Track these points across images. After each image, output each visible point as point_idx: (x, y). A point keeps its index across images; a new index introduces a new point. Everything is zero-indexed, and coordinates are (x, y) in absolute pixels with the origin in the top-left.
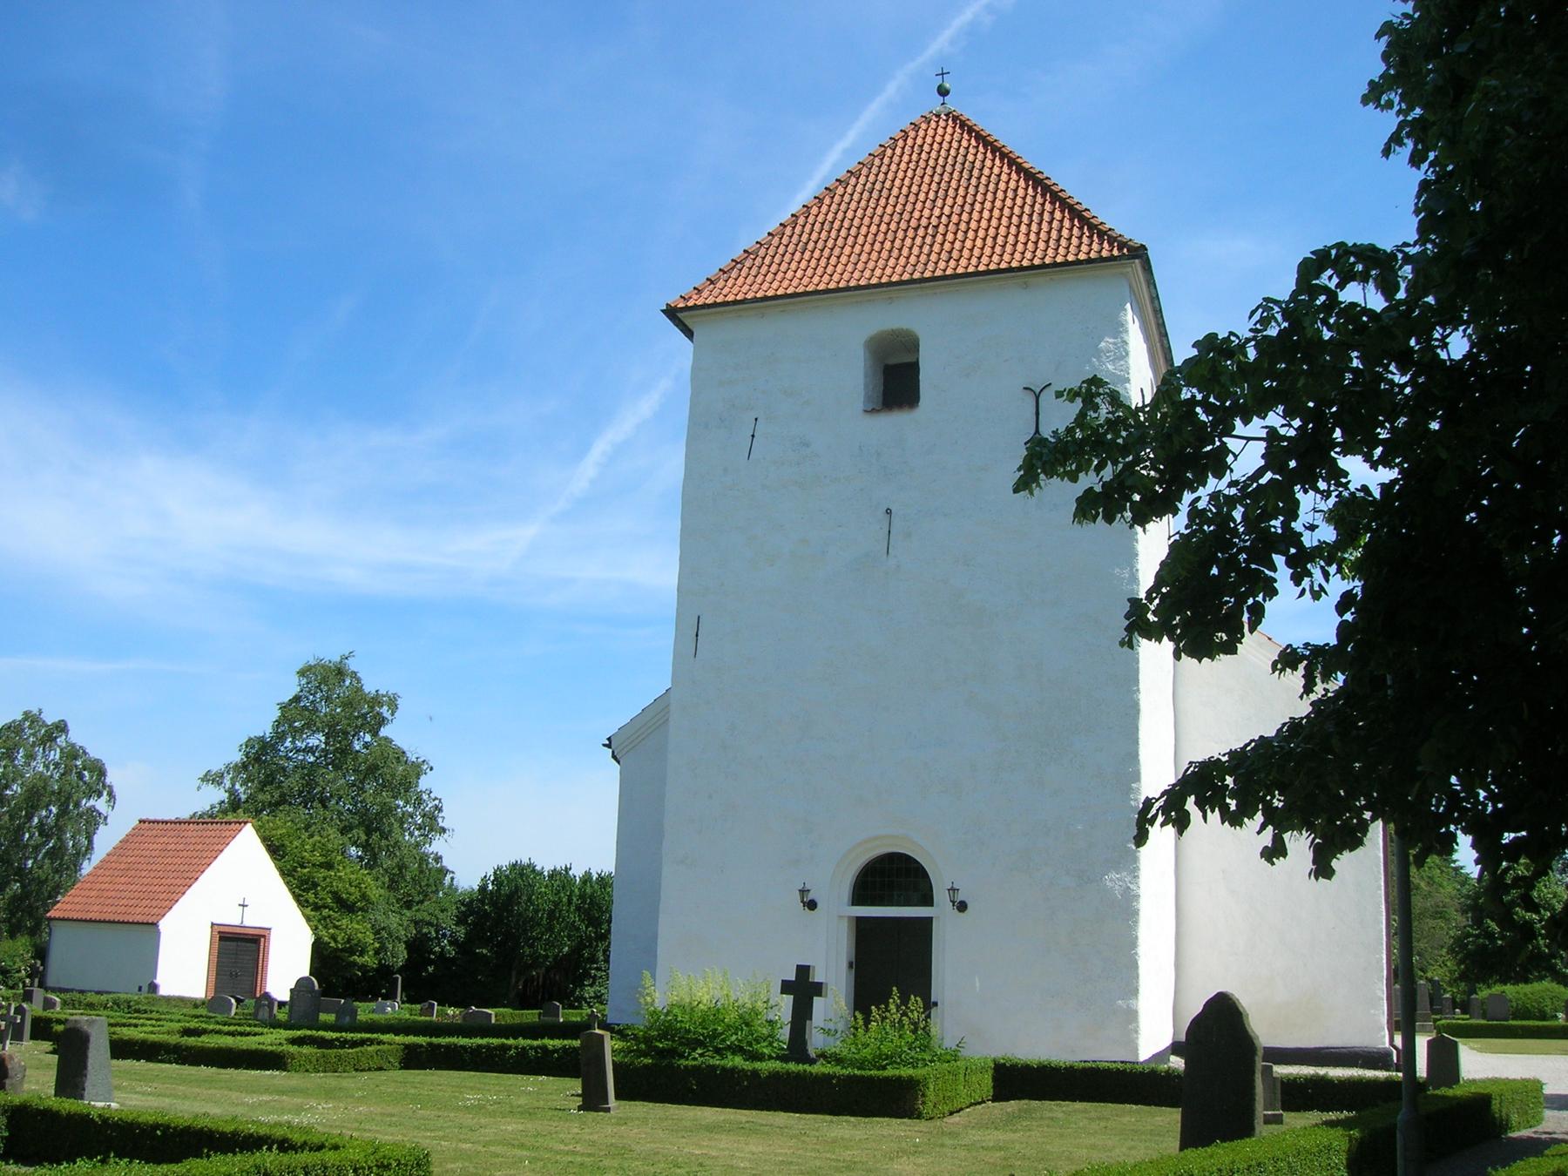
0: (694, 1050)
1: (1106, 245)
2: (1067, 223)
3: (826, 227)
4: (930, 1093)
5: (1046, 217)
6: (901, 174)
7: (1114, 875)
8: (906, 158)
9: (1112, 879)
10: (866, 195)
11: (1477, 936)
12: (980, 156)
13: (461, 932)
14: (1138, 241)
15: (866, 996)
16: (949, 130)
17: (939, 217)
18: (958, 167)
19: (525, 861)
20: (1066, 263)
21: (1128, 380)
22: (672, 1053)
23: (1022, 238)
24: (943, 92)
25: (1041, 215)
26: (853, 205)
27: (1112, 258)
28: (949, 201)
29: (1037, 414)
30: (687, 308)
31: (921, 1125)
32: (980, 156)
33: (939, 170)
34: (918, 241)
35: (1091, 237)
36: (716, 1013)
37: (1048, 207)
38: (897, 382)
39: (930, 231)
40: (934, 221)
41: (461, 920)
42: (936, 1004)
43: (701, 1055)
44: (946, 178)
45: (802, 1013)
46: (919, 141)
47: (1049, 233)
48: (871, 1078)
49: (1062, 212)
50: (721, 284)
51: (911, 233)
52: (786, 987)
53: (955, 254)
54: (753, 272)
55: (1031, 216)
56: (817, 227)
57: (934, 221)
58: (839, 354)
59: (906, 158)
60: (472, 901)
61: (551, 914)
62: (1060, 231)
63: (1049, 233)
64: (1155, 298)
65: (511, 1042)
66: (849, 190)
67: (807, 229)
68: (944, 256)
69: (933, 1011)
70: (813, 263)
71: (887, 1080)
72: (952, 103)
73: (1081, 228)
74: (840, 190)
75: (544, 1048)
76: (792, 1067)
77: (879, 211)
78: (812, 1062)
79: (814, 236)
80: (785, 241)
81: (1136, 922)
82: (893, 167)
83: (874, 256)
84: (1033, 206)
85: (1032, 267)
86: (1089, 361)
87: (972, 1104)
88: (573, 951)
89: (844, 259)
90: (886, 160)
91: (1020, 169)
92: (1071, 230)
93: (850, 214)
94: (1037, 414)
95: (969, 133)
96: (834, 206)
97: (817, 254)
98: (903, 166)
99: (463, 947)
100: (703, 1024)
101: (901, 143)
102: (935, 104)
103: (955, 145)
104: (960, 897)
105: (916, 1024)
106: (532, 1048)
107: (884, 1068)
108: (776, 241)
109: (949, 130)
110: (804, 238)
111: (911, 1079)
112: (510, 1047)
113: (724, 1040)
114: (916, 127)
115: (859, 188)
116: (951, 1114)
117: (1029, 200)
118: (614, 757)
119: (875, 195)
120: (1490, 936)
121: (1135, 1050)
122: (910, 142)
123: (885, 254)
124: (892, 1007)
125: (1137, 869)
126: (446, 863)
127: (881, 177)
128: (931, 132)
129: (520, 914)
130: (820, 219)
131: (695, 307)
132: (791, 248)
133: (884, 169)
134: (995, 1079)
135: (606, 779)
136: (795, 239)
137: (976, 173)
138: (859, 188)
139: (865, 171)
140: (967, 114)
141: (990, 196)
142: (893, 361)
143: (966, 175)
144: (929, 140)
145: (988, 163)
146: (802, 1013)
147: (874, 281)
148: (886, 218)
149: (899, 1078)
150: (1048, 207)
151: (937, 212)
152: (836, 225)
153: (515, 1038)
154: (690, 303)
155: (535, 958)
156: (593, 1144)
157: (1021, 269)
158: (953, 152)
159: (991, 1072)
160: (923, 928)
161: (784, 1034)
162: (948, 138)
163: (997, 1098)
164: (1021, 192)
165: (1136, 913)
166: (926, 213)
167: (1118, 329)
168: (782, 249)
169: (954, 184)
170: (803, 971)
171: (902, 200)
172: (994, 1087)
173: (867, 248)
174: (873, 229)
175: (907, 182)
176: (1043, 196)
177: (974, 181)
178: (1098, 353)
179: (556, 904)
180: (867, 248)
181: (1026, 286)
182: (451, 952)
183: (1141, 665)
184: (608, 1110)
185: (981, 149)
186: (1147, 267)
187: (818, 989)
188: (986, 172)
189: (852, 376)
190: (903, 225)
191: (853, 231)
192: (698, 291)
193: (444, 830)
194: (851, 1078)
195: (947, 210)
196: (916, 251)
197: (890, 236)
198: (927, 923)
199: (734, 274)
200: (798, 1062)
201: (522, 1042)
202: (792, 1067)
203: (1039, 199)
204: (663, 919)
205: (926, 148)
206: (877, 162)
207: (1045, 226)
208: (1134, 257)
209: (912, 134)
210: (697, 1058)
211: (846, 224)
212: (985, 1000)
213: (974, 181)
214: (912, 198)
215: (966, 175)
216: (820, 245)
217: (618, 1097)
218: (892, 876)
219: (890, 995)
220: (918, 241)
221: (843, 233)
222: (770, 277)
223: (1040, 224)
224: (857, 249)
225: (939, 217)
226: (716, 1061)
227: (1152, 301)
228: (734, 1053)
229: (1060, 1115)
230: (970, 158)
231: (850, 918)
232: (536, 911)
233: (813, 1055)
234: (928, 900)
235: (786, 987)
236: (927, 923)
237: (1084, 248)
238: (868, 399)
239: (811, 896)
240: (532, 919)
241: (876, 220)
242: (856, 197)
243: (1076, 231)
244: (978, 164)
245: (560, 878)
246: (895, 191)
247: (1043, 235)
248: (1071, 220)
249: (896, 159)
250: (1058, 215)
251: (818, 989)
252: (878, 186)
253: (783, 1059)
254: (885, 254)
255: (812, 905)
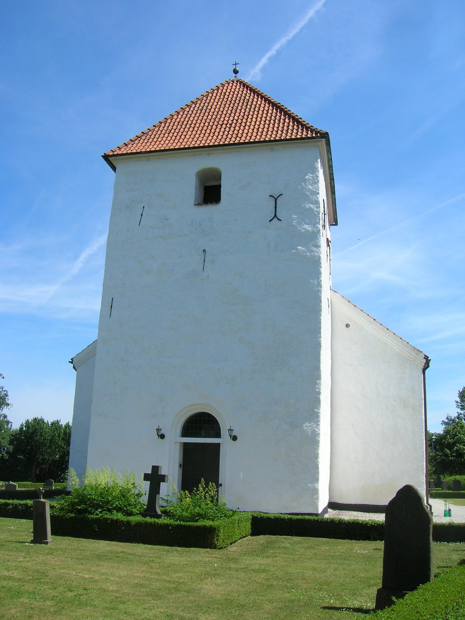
0: (97, 509)
1: (309, 132)
2: (291, 124)
3: (180, 124)
4: (221, 535)
5: (282, 121)
6: (215, 104)
7: (308, 424)
8: (218, 97)
9: (307, 426)
10: (199, 111)
11: (441, 456)
12: (252, 97)
13: (11, 448)
14: (325, 130)
15: (188, 483)
16: (238, 87)
17: (232, 121)
18: (242, 101)
19: (40, 417)
20: (291, 139)
21: (318, 194)
22: (85, 511)
23: (270, 129)
24: (236, 72)
25: (279, 120)
26: (193, 115)
27: (312, 138)
28: (237, 114)
29: (276, 208)
30: (114, 155)
31: (216, 553)
32: (252, 97)
33: (233, 102)
34: (223, 130)
35: (302, 130)
36: (107, 490)
37: (282, 117)
38: (210, 193)
39: (228, 126)
40: (230, 122)
41: (11, 443)
42: (221, 485)
43: (100, 512)
44: (236, 105)
45: (154, 491)
46: (224, 91)
47: (283, 127)
48: (190, 527)
49: (289, 119)
50: (130, 146)
51: (219, 126)
52: (147, 477)
53: (239, 135)
54: (146, 141)
55: (275, 121)
56: (176, 123)
57: (230, 122)
58: (184, 178)
59: (218, 97)
60: (16, 435)
61: (51, 441)
62: (288, 127)
63: (283, 127)
64: (330, 160)
65: (10, 501)
66: (192, 109)
67: (172, 124)
68: (234, 136)
69: (220, 488)
70: (173, 138)
71: (198, 528)
72: (239, 76)
73: (298, 126)
74: (187, 109)
75: (26, 505)
76: (148, 519)
77: (205, 118)
78: (159, 517)
79: (175, 127)
80: (161, 129)
81: (318, 447)
82: (212, 101)
83: (202, 135)
84: (275, 117)
85: (275, 141)
86: (301, 184)
87: (241, 538)
88: (60, 457)
89: (188, 137)
90: (209, 98)
91: (270, 102)
92: (293, 126)
93: (191, 119)
94: (276, 208)
95: (247, 88)
96: (184, 116)
97: (175, 134)
98: (216, 100)
99: (12, 455)
100: (101, 494)
101: (216, 91)
102: (232, 76)
103: (240, 93)
104: (234, 434)
105: (212, 497)
106: (20, 505)
107: (197, 521)
108: (157, 129)
109: (238, 87)
110: (170, 128)
111: (211, 527)
112: (9, 504)
113: (112, 504)
114: (223, 85)
115: (196, 109)
116: (231, 544)
117: (274, 114)
118: (74, 368)
119: (203, 111)
120: (446, 455)
121: (317, 508)
122: (220, 91)
123: (207, 135)
124: (201, 489)
125: (319, 421)
126: (9, 418)
127: (206, 104)
128: (229, 88)
129: (37, 441)
130: (178, 120)
131: (118, 155)
132: (163, 132)
133: (208, 101)
134: (252, 524)
135: (70, 378)
136: (166, 128)
137: (250, 103)
138: (196, 109)
139: (199, 102)
140: (247, 80)
141: (256, 113)
142: (209, 184)
143: (245, 104)
144: (229, 91)
145: (255, 100)
146: (154, 491)
147: (202, 145)
148: (208, 121)
149: (205, 527)
150: (282, 117)
151: (231, 118)
152: (185, 123)
153: (13, 499)
154: (116, 153)
155: (43, 460)
156: (26, 570)
157: (270, 141)
158: (239, 95)
159: (250, 521)
160: (215, 449)
161: (144, 500)
162: (237, 90)
163: (253, 534)
164: (270, 111)
165: (318, 442)
166: (227, 119)
167: (314, 170)
168: (159, 132)
169: (239, 108)
170: (155, 469)
171: (215, 113)
172: (252, 528)
173: (199, 132)
174: (202, 125)
175: (218, 106)
176: (280, 113)
177: (249, 107)
178: (305, 181)
179: (53, 437)
180: (199, 132)
181: (272, 150)
182: (6, 457)
183: (322, 325)
184: (47, 543)
185: (252, 94)
186: (328, 143)
187: (163, 478)
188: (254, 103)
189: (190, 189)
190: (216, 123)
191: (193, 125)
192: (120, 148)
193: (8, 404)
194: (178, 526)
195: (236, 118)
196: (221, 133)
197: (210, 127)
198: (218, 446)
199: (137, 142)
200: (151, 517)
201: (16, 502)
202: (148, 519)
203: (278, 114)
204: (90, 442)
205: (227, 93)
206: (205, 98)
207: (281, 125)
208: (323, 138)
209: (221, 88)
210: (98, 514)
211: (190, 123)
212: (247, 484)
213: (249, 107)
214: (220, 113)
215: (245, 104)
216: (177, 131)
217: (52, 534)
218: (201, 423)
219: (200, 482)
220: (223, 130)
221: (188, 126)
222: (153, 143)
223: (279, 124)
224: (194, 133)
225: (232, 121)
226: (108, 516)
227: (329, 162)
228: (118, 511)
229: (288, 545)
230: (247, 98)
231: (180, 443)
232: (44, 440)
233: (159, 513)
234: (218, 435)
235: (147, 477)
236: (218, 446)
237: (299, 134)
238: (196, 199)
239: (162, 432)
240: (42, 443)
241: (203, 121)
242: (195, 112)
243: (295, 127)
244: (251, 100)
245: (56, 424)
246: (212, 110)
247: (280, 128)
248: (293, 123)
249: (213, 98)
250: (287, 120)
251: (163, 478)
252: (205, 108)
253: (144, 515)
254: (207, 135)
255: (162, 436)
